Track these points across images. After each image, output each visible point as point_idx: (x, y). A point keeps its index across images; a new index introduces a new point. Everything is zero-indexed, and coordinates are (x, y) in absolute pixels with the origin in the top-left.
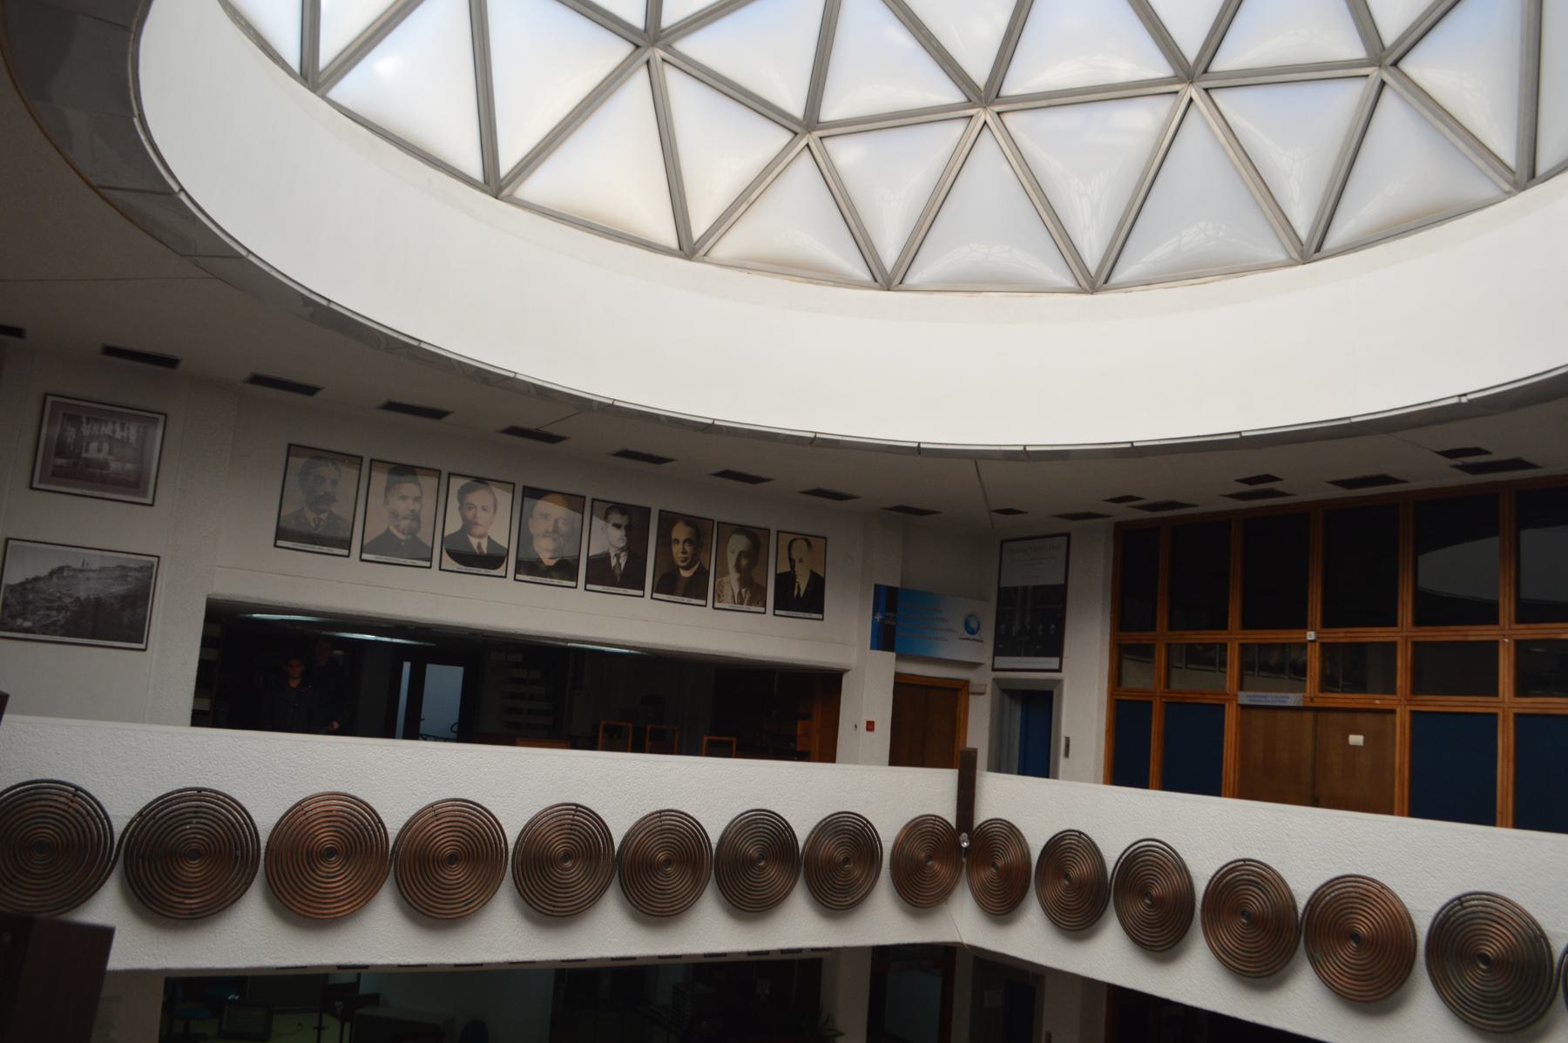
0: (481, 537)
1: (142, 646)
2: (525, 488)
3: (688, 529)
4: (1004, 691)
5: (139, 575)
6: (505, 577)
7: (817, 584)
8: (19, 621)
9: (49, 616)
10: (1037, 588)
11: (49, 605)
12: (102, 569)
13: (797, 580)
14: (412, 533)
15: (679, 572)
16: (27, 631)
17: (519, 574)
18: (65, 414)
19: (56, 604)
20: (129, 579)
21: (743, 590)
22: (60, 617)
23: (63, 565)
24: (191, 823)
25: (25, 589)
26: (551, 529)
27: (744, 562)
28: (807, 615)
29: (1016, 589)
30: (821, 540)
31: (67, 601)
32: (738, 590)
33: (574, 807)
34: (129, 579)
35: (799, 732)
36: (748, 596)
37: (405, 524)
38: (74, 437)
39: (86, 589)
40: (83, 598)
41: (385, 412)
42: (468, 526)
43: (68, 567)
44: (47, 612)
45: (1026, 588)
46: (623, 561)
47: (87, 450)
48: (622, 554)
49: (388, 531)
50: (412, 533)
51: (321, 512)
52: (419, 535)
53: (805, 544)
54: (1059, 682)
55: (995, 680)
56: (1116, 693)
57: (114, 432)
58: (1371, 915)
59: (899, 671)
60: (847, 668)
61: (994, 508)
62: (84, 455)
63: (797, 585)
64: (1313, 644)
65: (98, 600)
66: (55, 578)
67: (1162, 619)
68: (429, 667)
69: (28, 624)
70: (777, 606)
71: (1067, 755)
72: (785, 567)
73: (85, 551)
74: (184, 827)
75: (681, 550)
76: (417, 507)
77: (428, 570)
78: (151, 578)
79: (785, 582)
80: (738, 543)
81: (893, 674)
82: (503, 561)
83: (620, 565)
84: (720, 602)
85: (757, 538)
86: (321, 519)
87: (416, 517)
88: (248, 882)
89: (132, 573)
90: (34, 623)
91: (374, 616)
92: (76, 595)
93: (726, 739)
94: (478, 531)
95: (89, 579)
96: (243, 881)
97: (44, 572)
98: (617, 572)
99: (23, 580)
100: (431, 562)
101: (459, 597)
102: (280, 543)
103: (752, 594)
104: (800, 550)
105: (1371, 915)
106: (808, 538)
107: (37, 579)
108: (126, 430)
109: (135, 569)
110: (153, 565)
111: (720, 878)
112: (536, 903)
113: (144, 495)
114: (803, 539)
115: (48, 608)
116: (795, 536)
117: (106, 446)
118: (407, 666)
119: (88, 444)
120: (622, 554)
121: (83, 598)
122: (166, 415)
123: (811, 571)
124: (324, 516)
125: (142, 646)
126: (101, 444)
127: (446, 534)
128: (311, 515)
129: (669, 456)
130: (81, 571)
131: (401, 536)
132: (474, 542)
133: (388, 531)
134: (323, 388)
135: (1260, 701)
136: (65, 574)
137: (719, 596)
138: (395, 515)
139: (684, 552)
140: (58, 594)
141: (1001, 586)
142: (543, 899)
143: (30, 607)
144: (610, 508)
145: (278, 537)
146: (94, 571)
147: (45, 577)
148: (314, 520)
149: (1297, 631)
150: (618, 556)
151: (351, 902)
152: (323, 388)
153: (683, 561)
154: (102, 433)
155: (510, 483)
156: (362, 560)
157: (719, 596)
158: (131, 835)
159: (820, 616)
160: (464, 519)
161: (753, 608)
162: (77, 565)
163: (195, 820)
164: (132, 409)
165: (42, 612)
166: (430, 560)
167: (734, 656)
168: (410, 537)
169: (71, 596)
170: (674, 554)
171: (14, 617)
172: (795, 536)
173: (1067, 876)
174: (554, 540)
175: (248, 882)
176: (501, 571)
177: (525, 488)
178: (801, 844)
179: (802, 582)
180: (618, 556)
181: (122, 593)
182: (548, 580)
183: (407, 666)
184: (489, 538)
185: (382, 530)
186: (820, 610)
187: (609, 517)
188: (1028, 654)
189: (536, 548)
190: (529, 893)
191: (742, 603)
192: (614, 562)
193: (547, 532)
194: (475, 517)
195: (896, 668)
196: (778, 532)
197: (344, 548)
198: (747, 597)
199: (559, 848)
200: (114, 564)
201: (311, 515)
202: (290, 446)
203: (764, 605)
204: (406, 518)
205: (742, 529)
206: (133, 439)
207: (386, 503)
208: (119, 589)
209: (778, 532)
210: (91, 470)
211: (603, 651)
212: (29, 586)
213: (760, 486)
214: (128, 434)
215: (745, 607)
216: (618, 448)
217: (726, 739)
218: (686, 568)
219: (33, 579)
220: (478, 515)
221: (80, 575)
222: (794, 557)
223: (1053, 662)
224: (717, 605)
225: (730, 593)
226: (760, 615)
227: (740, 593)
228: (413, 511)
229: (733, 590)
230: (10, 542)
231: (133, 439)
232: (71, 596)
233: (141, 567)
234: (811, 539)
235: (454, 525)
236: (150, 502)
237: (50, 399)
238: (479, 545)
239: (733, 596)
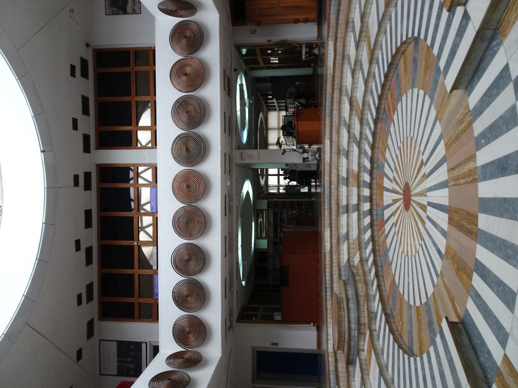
10: (118, 356)
29: (118, 366)
45: (118, 361)
56: (155, 319)
58: (193, 62)
64: (138, 243)
67: (129, 271)
105: (193, 62)
112: (198, 64)
135: (155, 261)
141: (116, 374)
149: (135, 257)
199: (184, 78)
223: (144, 345)
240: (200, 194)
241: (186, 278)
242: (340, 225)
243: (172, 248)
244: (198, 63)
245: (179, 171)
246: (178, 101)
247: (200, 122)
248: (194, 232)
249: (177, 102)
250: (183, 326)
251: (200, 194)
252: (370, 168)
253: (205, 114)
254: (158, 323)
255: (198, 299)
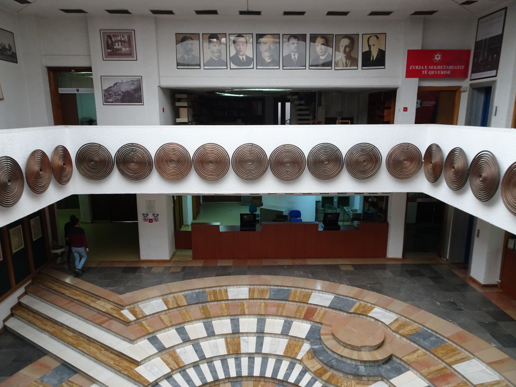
0: (243, 55)
1: (142, 104)
2: (257, 35)
3: (323, 40)
4: (474, 89)
5: (137, 82)
6: (253, 68)
7: (382, 54)
8: (109, 100)
9: (116, 97)
11: (116, 94)
12: (127, 82)
13: (372, 54)
14: (219, 57)
15: (319, 57)
16: (112, 102)
17: (258, 66)
18: (106, 35)
19: (117, 94)
20: (135, 84)
21: (347, 61)
22: (119, 98)
23: (117, 82)
24: (131, 153)
25: (109, 90)
26: (268, 49)
27: (347, 50)
28: (377, 67)
30: (384, 35)
31: (120, 92)
32: (345, 61)
33: (374, 147)
34: (135, 84)
35: (385, 114)
36: (350, 63)
37: (216, 54)
38: (111, 42)
39: (124, 88)
40: (124, 91)
41: (371, 17)
42: (238, 52)
43: (118, 82)
44: (116, 96)
45: (486, 39)
46: (296, 56)
47: (115, 46)
48: (296, 54)
49: (211, 58)
50: (219, 57)
51: (190, 55)
52: (222, 58)
53: (376, 38)
54: (494, 82)
55: (471, 85)
57: (121, 38)
59: (420, 85)
60: (398, 87)
61: (460, 3)
62: (115, 47)
63: (372, 56)
65: (128, 91)
66: (115, 86)
68: (286, 103)
69: (111, 100)
70: (363, 65)
71: (495, 115)
72: (366, 49)
73: (124, 77)
74: (129, 155)
75: (320, 49)
76: (220, 48)
77: (356, 70)
78: (140, 83)
79: (367, 56)
80: (345, 42)
81: (417, 87)
82: (252, 63)
83: (295, 58)
84: (337, 67)
85: (353, 39)
86: (189, 57)
87: (220, 51)
88: (151, 169)
89: (135, 82)
90: (113, 100)
91: (205, 88)
92: (122, 91)
93: (347, 121)
94: (242, 53)
95: (124, 85)
96: (149, 169)
97: (112, 85)
98: (294, 61)
99: (107, 88)
100: (200, 66)
101: (204, 77)
102: (178, 67)
103: (352, 61)
104: (373, 41)
106: (377, 35)
107: (111, 87)
108: (124, 38)
109: (136, 81)
110: (140, 79)
111: (17, 165)
113: (105, 57)
114: (375, 36)
115: (116, 95)
116: (371, 35)
117: (120, 43)
118: (280, 104)
119: (115, 44)
120: (296, 54)
121: (124, 91)
122: (134, 30)
123: (379, 49)
124: (190, 56)
125: (142, 104)
126: (118, 43)
127: (231, 56)
128: (186, 57)
129: (87, 11)
130: (122, 83)
131: (215, 59)
132: (241, 57)
133: (211, 58)
134: (350, 12)
136: (118, 85)
137: (337, 65)
138: (213, 52)
139: (321, 49)
140: (117, 91)
142: (145, 174)
143: (111, 95)
144: (290, 37)
145: (177, 66)
146: (124, 83)
147: (113, 86)
148: (188, 58)
150: (294, 55)
151: (181, 175)
152: (350, 12)
153: (321, 53)
154: (118, 40)
155: (100, 31)
156: (177, 68)
157: (337, 65)
158: (117, 157)
159: (383, 67)
160: (236, 49)
161: (352, 68)
162: (120, 82)
163: (132, 153)
164: (107, 30)
165: (114, 97)
166: (305, 66)
167: (345, 87)
168: (219, 59)
169: (120, 91)
170: (317, 51)
171: (108, 99)
172: (371, 35)
173: (454, 168)
174: (269, 52)
175: (151, 169)
176: (251, 66)
177: (257, 35)
178: (344, 156)
179: (375, 54)
180: (294, 55)
181: (134, 88)
182: (269, 67)
183: (280, 104)
184: (246, 55)
185: (209, 58)
186: (384, 65)
187: (290, 40)
188: (484, 71)
189: (263, 56)
190: (396, 175)
191: (347, 66)
192: (293, 57)
193: (267, 49)
194: (240, 48)
195: (419, 84)
196: (283, 35)
197: (198, 66)
198: (349, 64)
200: (130, 80)
201: (186, 57)
202: (176, 34)
203: (357, 66)
204: (216, 52)
205: (346, 36)
206: (127, 40)
207: (209, 48)
208: (133, 87)
209: (283, 35)
210: (118, 52)
211: (262, 91)
212: (109, 89)
213: (434, 15)
214: (125, 38)
215: (348, 68)
216: (413, 12)
217: (347, 121)
218: (322, 56)
219: (110, 87)
220: (241, 47)
221: (122, 84)
222: (370, 44)
223: (493, 73)
224: (336, 68)
225: (342, 64)
226: (330, 70)
227: (346, 62)
228: (218, 50)
229: (343, 61)
230: (102, 77)
231: (127, 40)
232: (120, 91)
233: (137, 80)
234: (378, 35)
235: (233, 52)
236: (136, 59)
237: (101, 31)
238: (243, 58)
239: (343, 64)
240: (279, 172)
241: (113, 159)
242: (242, 316)
243: (301, 146)
244: (398, 171)
245: (381, 154)
246: (338, 150)
247: (317, 171)
248: (283, 169)
249: (337, 149)
250: (197, 159)
251: (279, 172)
252: (135, 318)
253: (358, 179)
254: (512, 128)
255: (178, 170)
